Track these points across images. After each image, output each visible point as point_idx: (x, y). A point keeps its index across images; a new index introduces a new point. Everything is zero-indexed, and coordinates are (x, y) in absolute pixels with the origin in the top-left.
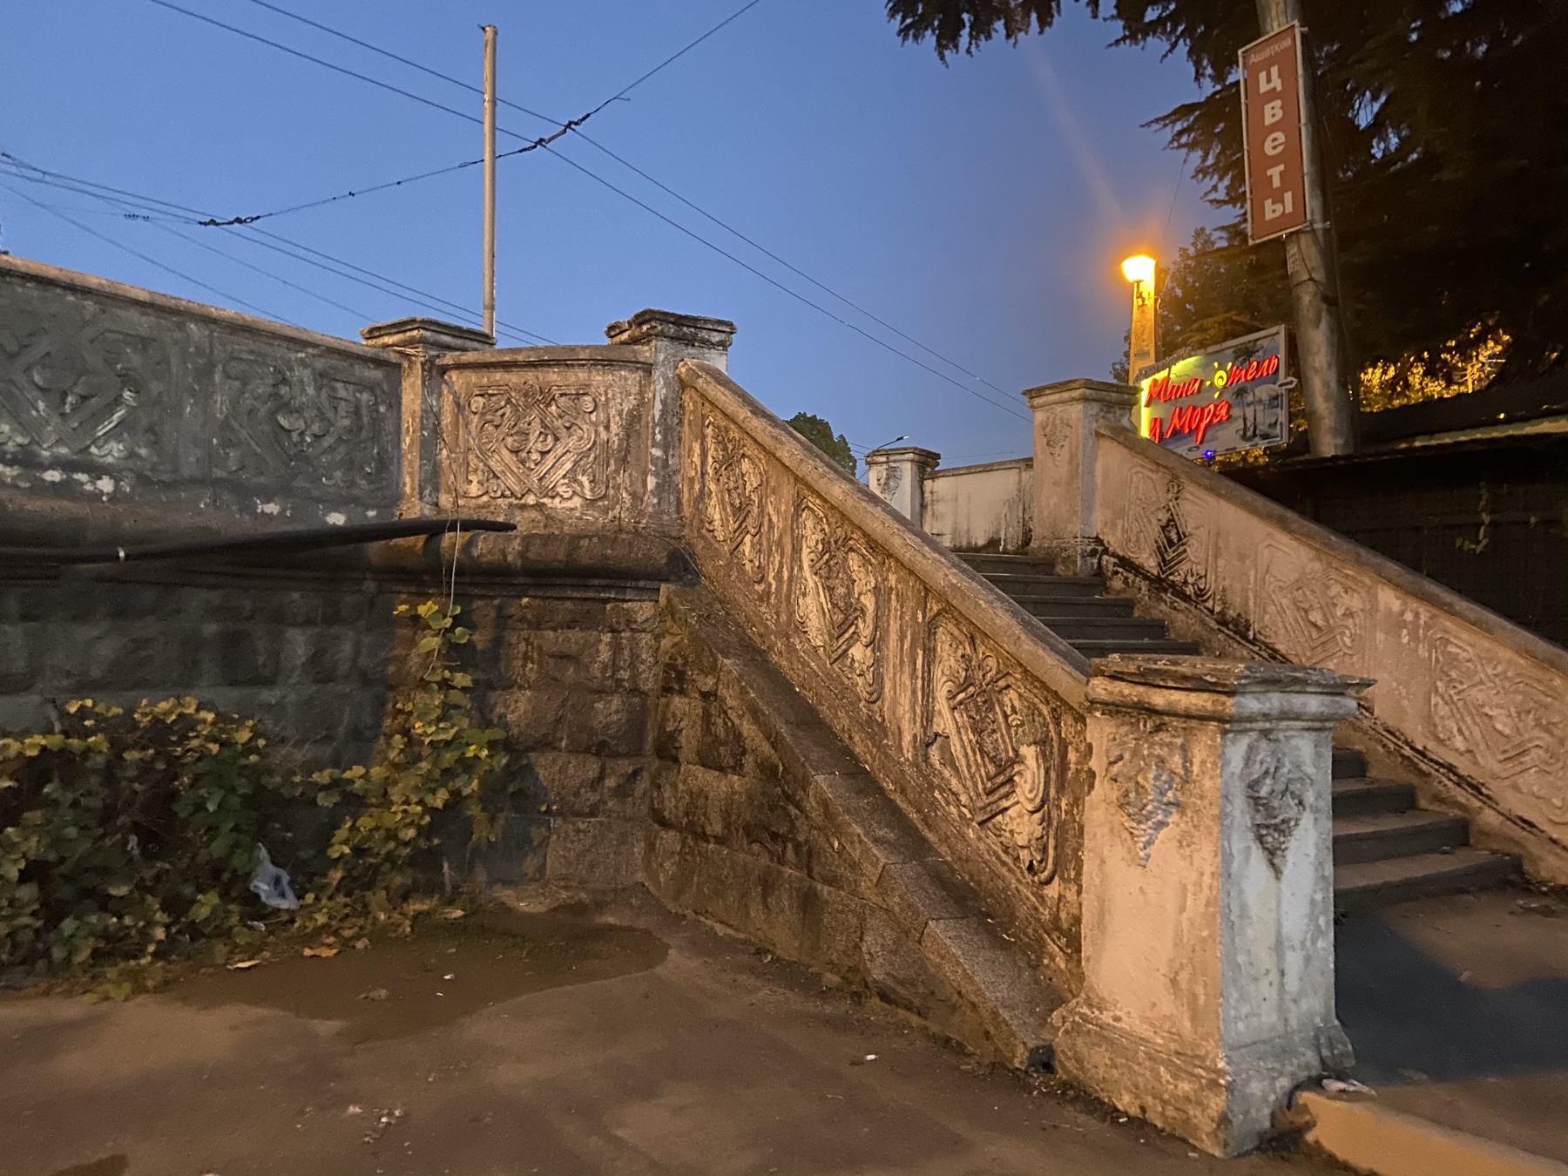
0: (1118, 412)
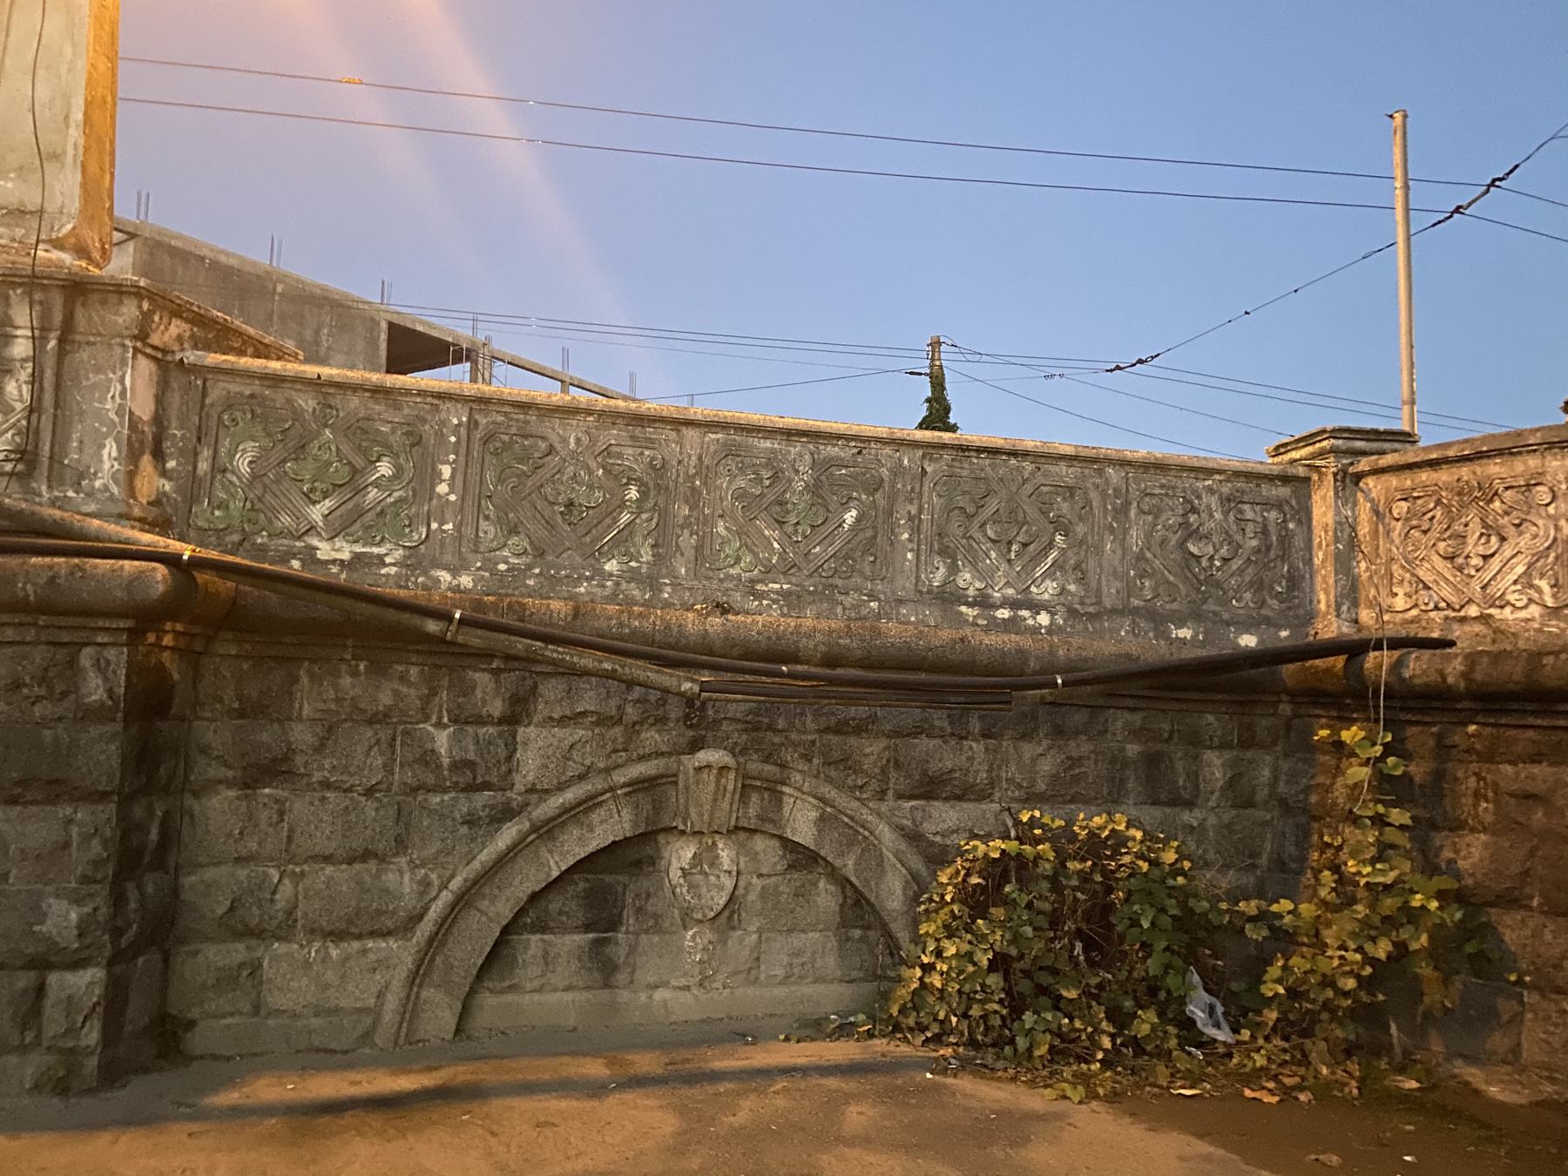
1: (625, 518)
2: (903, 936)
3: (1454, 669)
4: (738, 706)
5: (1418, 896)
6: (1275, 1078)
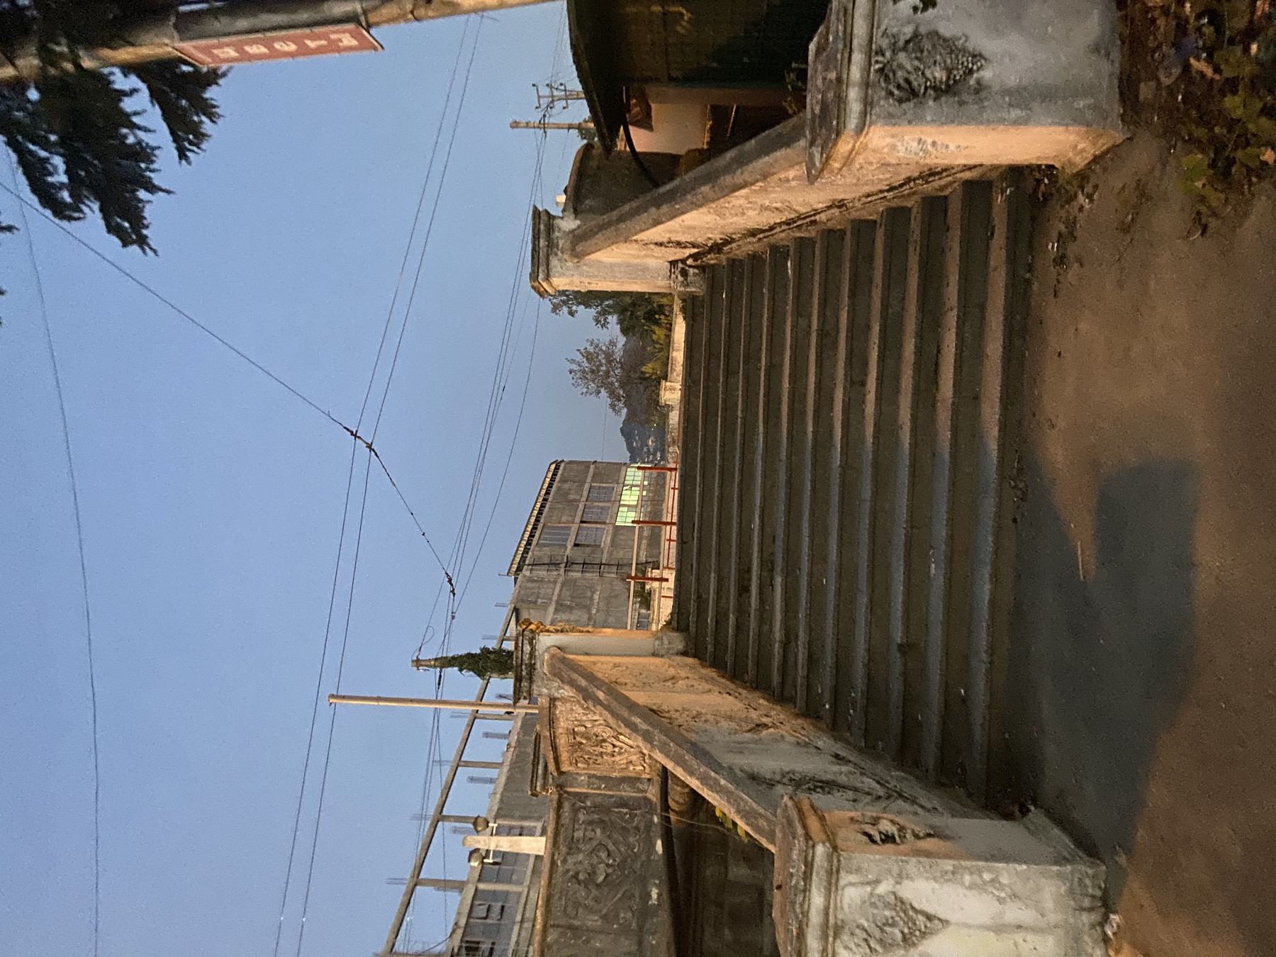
0: (557, 234)
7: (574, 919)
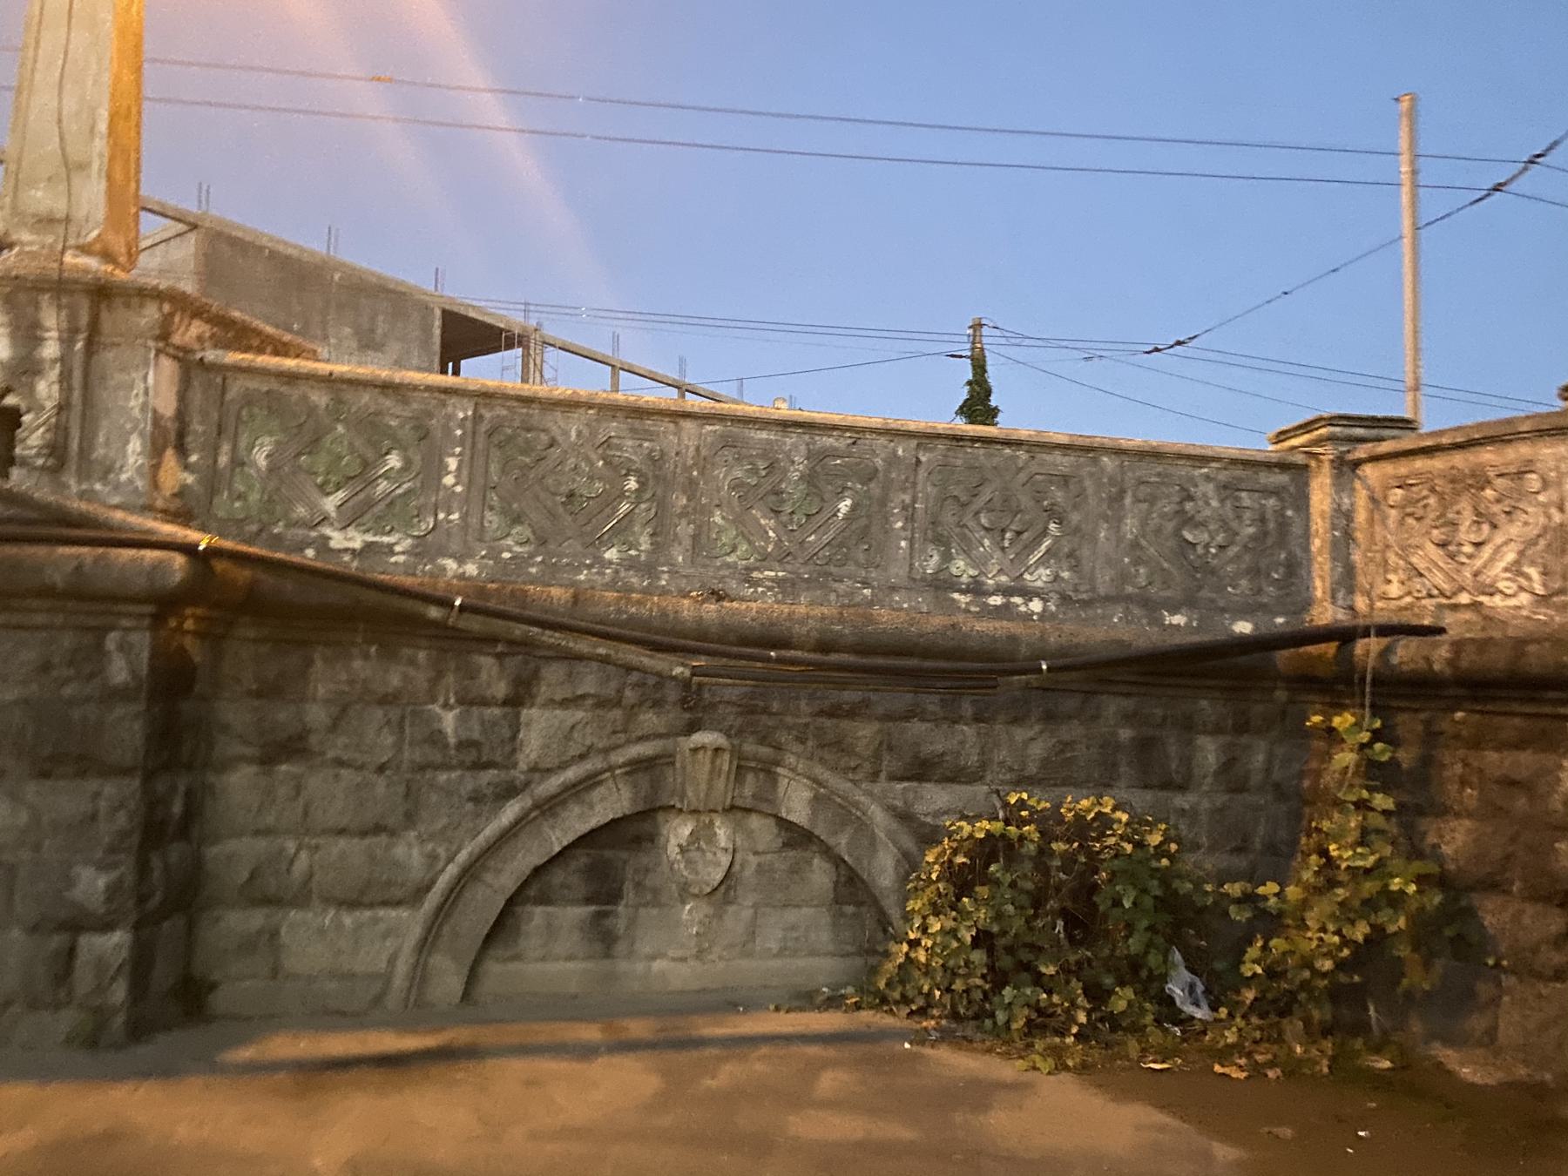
1: (624, 507)
2: (894, 914)
3: (1440, 655)
4: (733, 691)
5: (1397, 880)
6: (1249, 1055)
7: (1134, 496)
